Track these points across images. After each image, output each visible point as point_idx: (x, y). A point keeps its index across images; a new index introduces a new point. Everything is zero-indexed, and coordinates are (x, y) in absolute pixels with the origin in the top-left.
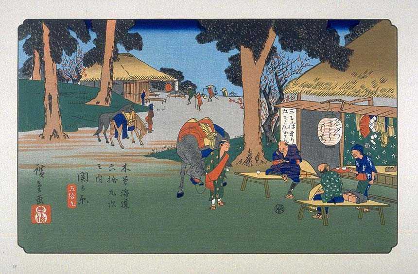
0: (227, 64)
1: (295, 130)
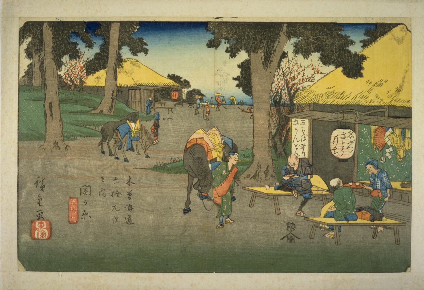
0: (237, 72)
1: (306, 143)
